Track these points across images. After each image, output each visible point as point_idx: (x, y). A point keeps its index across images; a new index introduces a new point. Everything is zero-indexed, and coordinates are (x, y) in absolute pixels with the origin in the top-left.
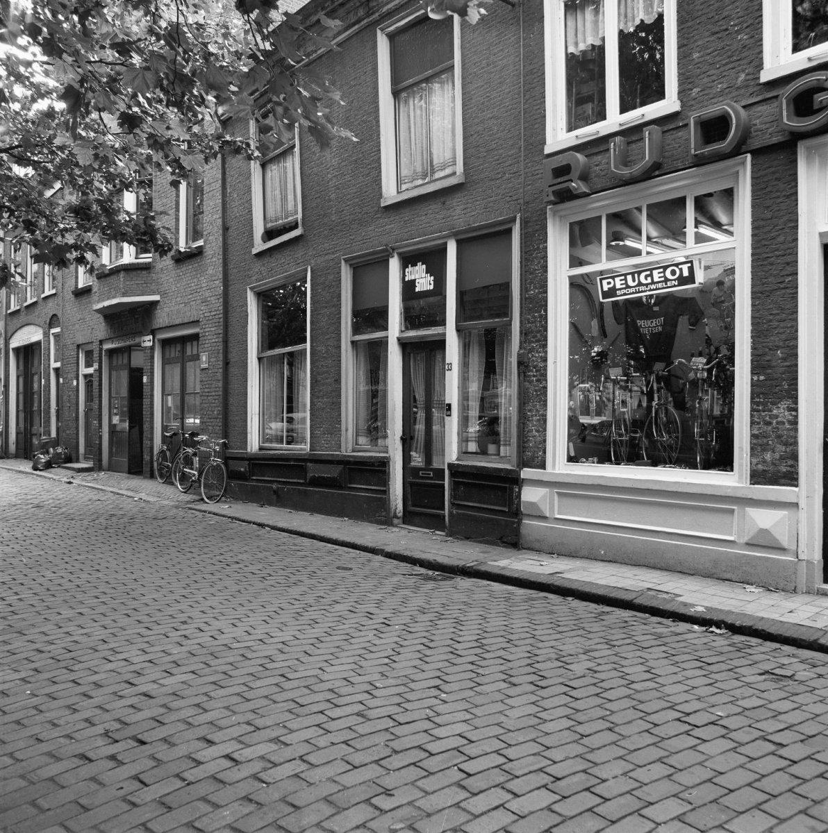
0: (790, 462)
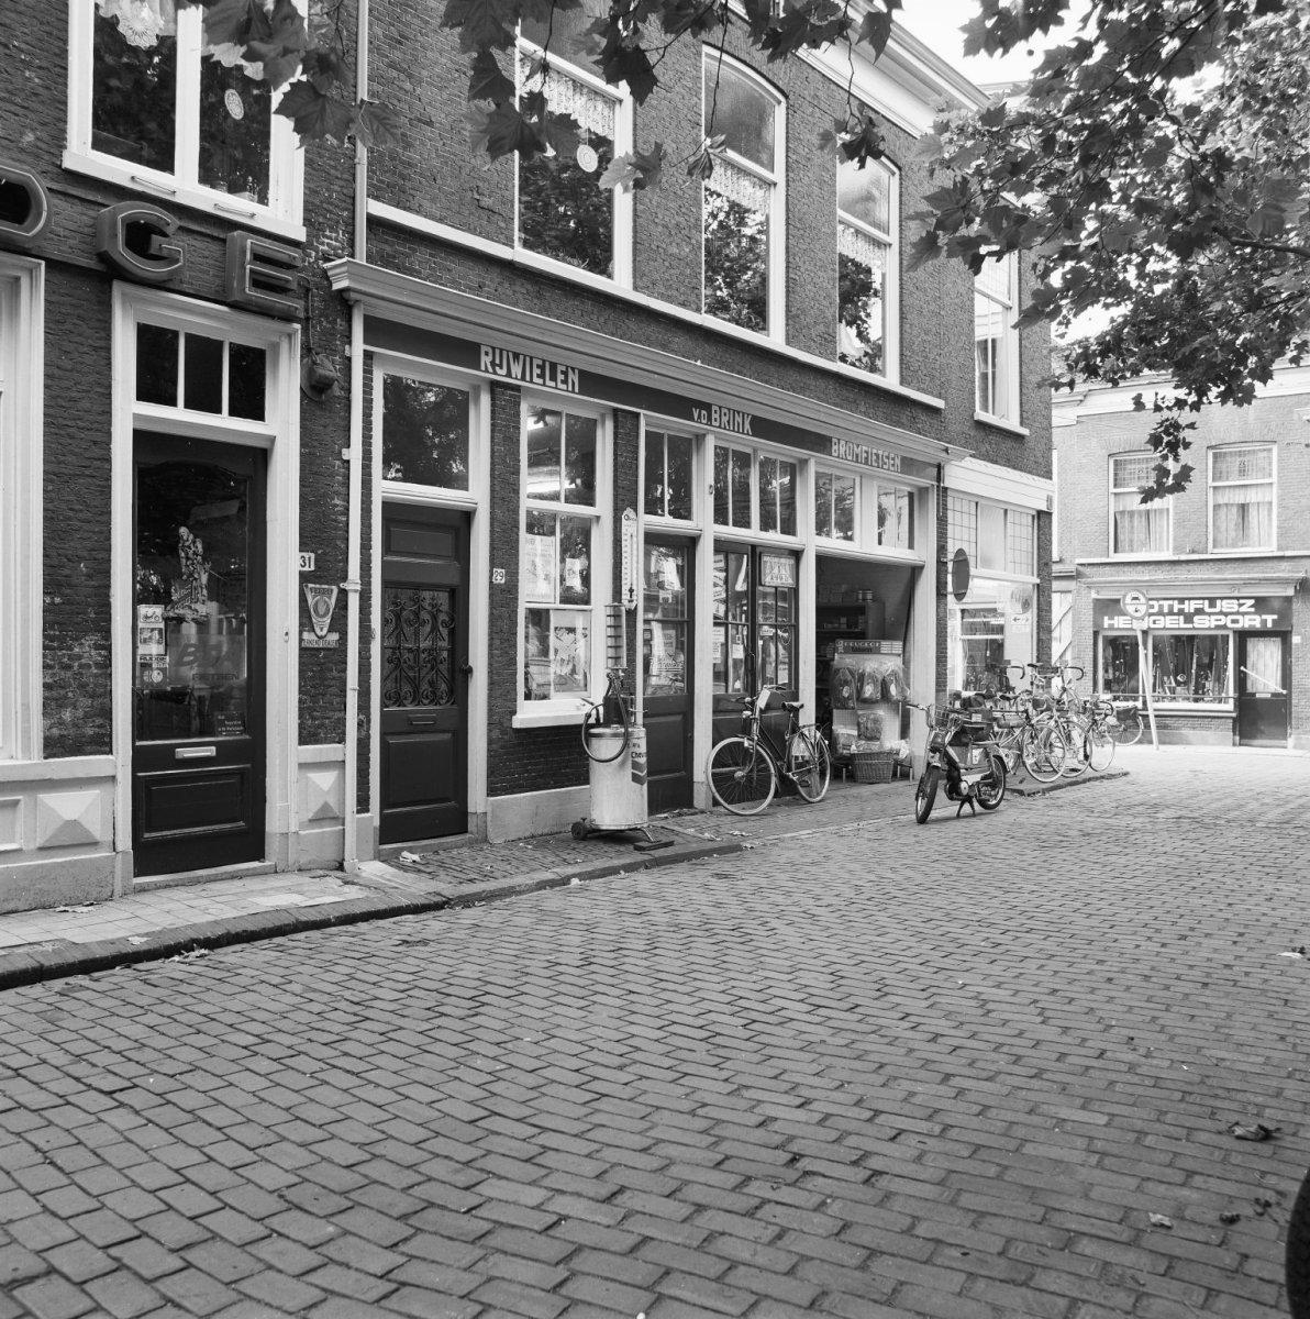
0: (99, 721)
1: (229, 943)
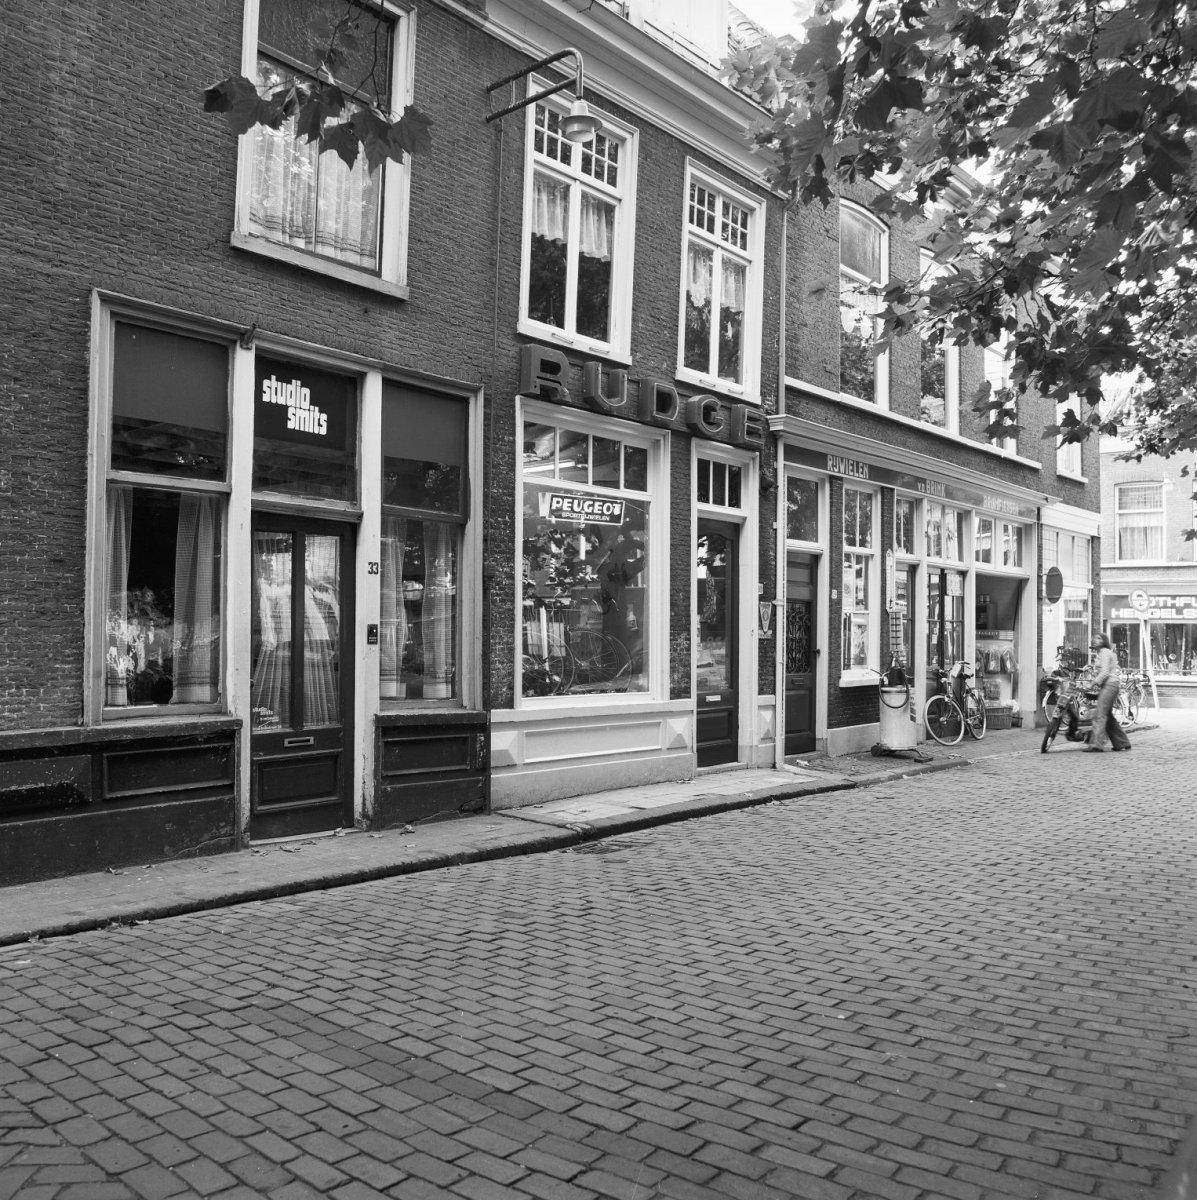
1: (676, 820)
